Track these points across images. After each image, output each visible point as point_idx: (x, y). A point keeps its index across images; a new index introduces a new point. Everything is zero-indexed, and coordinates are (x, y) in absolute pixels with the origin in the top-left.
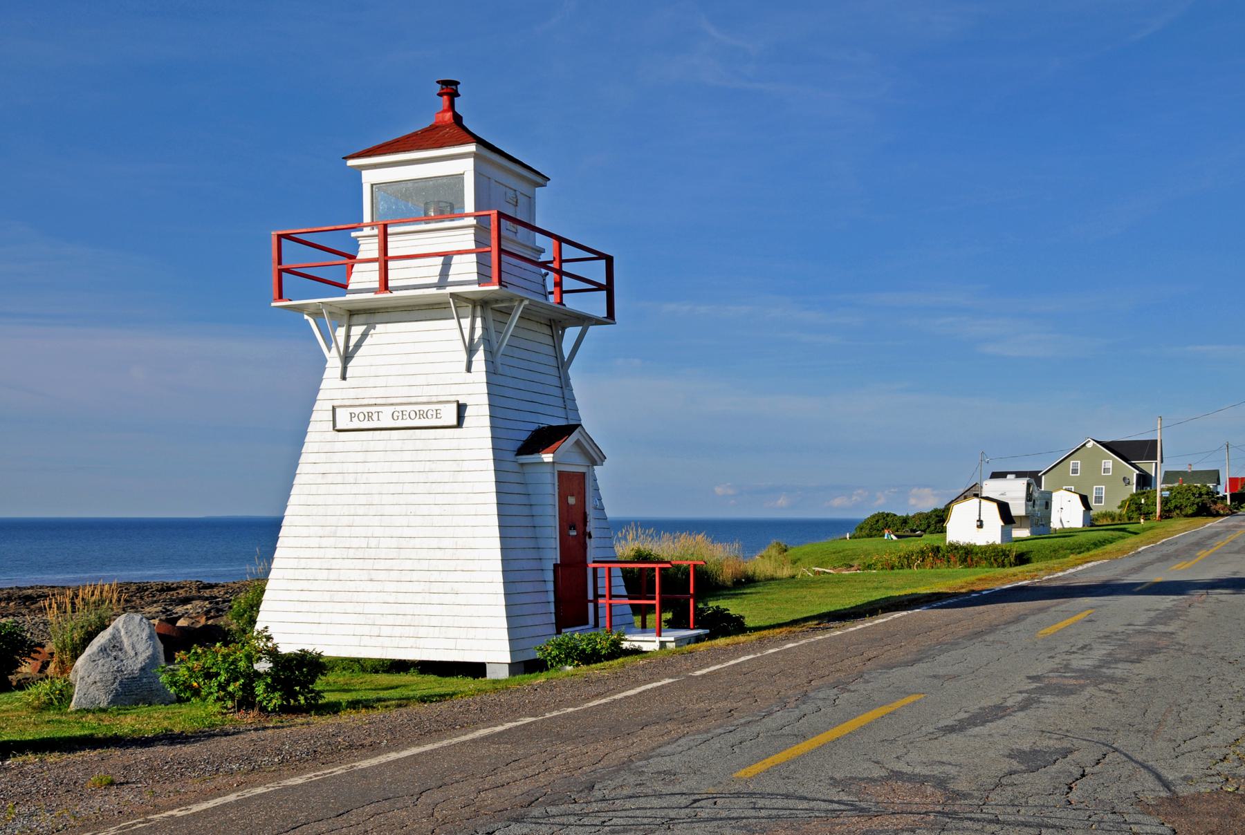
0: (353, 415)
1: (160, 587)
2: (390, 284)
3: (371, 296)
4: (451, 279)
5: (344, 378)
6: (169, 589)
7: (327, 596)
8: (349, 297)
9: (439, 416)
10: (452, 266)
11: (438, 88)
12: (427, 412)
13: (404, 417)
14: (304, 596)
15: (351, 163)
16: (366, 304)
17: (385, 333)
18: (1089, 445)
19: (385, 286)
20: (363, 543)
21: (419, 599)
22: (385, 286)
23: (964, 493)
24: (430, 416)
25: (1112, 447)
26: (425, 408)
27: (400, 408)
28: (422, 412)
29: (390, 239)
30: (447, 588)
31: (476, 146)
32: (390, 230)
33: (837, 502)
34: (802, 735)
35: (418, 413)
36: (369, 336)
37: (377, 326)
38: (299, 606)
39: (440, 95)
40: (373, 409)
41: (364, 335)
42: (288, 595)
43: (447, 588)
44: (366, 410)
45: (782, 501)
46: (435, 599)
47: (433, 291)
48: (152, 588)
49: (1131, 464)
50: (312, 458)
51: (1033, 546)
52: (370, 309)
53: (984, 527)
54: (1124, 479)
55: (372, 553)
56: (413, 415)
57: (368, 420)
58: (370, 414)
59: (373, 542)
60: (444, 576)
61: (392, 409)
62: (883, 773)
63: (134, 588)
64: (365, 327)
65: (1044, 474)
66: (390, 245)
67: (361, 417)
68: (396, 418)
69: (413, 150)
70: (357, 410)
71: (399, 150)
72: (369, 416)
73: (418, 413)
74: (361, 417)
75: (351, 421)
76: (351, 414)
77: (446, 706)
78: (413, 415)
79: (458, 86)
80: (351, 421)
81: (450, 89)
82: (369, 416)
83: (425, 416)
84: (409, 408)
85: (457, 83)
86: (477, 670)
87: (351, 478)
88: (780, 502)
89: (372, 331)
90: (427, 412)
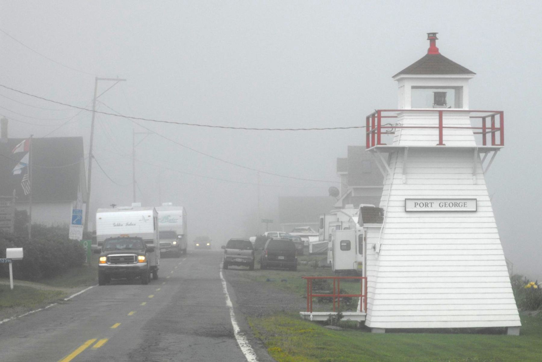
0: (416, 204)
9: (465, 206)
12: (420, 204)
23: (324, 235)
26: (458, 202)
27: (444, 202)
28: (456, 204)
31: (68, 234)
34: (281, 345)
40: (429, 202)
44: (424, 202)
51: (359, 271)
56: (451, 205)
57: (426, 207)
58: (427, 204)
61: (439, 202)
62: (97, 96)
67: (421, 205)
68: (441, 206)
70: (419, 202)
72: (427, 205)
75: (415, 207)
76: (415, 203)
77: (307, 330)
78: (451, 205)
80: (415, 207)
83: (458, 205)
90: (420, 204)
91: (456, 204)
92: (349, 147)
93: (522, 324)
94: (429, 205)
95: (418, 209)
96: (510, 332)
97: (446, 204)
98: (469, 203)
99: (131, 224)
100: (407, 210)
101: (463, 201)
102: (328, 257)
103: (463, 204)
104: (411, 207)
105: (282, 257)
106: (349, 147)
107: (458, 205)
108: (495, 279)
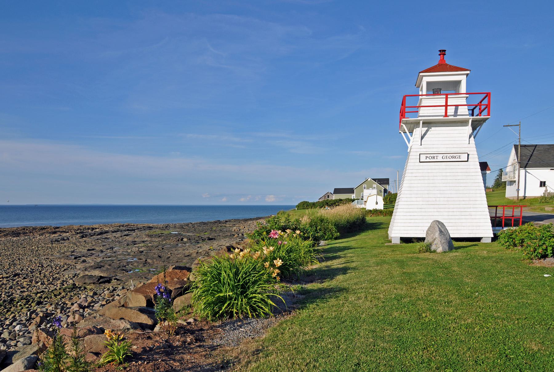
0: (427, 157)
1: (40, 228)
2: (448, 114)
3: (442, 118)
4: (458, 113)
5: (421, 145)
6: (44, 229)
7: (421, 217)
8: (458, 117)
9: (460, 158)
10: (459, 109)
11: (439, 53)
13: (447, 158)
14: (412, 217)
15: (421, 74)
16: (431, 121)
17: (435, 131)
18: (369, 180)
19: (446, 115)
20: (434, 199)
21: (457, 217)
22: (446, 115)
24: (456, 158)
25: (375, 180)
26: (455, 155)
27: (445, 155)
28: (454, 157)
29: (448, 99)
30: (467, 213)
32: (449, 96)
33: (242, 199)
35: (452, 157)
36: (429, 131)
37: (432, 128)
38: (409, 221)
39: (440, 55)
41: (427, 131)
42: (405, 217)
43: (467, 213)
44: (432, 155)
45: (224, 199)
46: (463, 217)
47: (452, 117)
48: (38, 228)
49: (382, 186)
50: (410, 171)
52: (428, 122)
53: (378, 204)
54: (380, 190)
55: (438, 203)
56: (450, 157)
58: (434, 157)
59: (438, 199)
60: (466, 210)
63: (31, 228)
64: (427, 128)
65: (355, 189)
66: (448, 101)
67: (430, 158)
68: (443, 158)
69: (446, 71)
70: (428, 155)
71: (428, 71)
72: (434, 158)
73: (452, 157)
74: (430, 158)
79: (446, 52)
81: (443, 52)
82: (434, 158)
83: (455, 157)
84: (448, 155)
85: (445, 51)
86: (479, 239)
87: (427, 178)
88: (223, 200)
89: (430, 130)
91: (434, 157)
92: (427, 82)
93: (494, 235)
94: (436, 158)
95: (428, 160)
96: (483, 241)
97: (447, 157)
98: (462, 155)
99: (44, 229)
100: (467, 160)
101: (459, 155)
102: (394, 211)
103: (445, 157)
104: (423, 158)
105: (370, 222)
106: (427, 82)
107: (455, 157)
108: (407, 207)
